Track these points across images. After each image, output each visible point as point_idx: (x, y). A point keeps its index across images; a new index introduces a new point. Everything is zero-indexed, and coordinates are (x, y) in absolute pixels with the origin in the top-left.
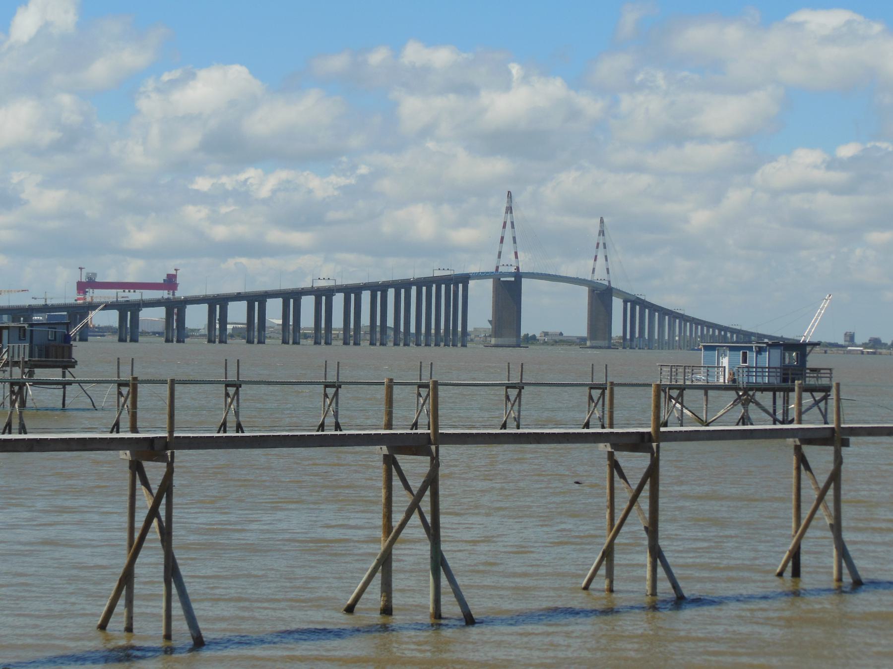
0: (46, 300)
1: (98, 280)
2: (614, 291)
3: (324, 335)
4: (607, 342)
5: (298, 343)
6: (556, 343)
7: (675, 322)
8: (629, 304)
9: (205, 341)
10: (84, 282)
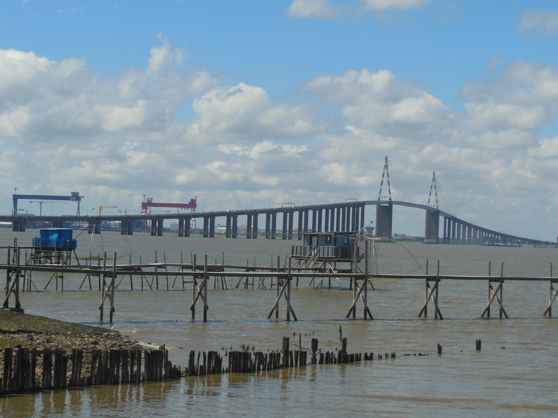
0: (126, 212)
1: (153, 202)
2: (440, 212)
3: (271, 234)
4: (436, 240)
5: (275, 239)
6: (403, 240)
7: (477, 232)
8: (447, 219)
9: (225, 237)
10: (145, 203)
